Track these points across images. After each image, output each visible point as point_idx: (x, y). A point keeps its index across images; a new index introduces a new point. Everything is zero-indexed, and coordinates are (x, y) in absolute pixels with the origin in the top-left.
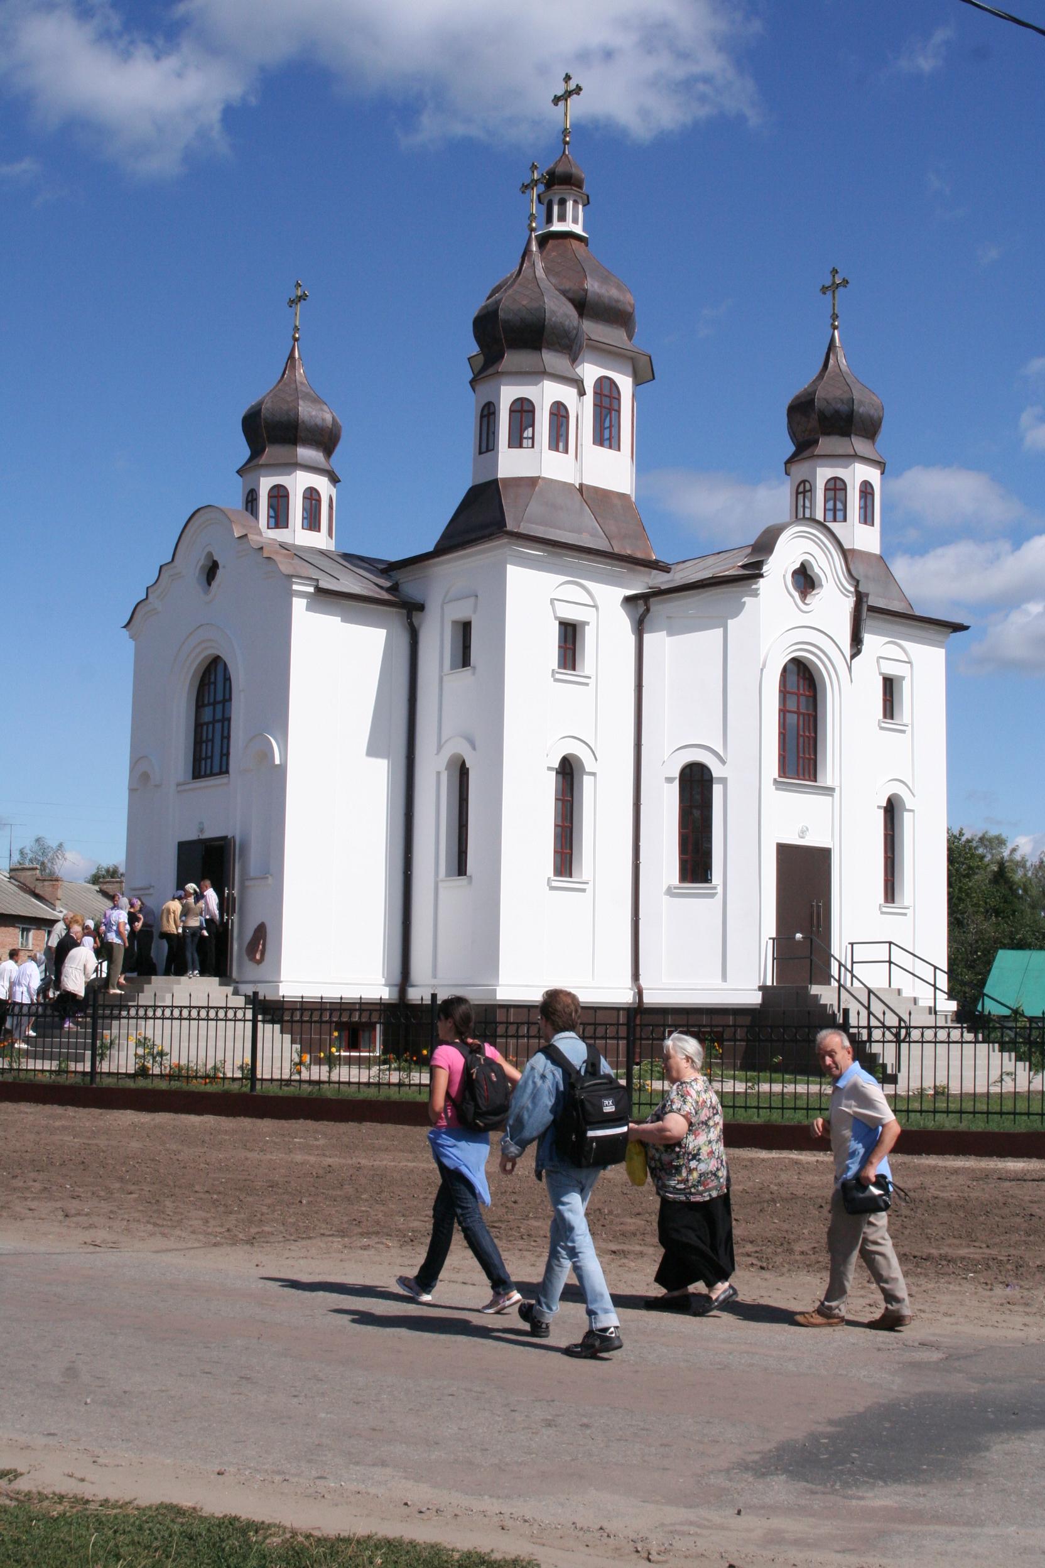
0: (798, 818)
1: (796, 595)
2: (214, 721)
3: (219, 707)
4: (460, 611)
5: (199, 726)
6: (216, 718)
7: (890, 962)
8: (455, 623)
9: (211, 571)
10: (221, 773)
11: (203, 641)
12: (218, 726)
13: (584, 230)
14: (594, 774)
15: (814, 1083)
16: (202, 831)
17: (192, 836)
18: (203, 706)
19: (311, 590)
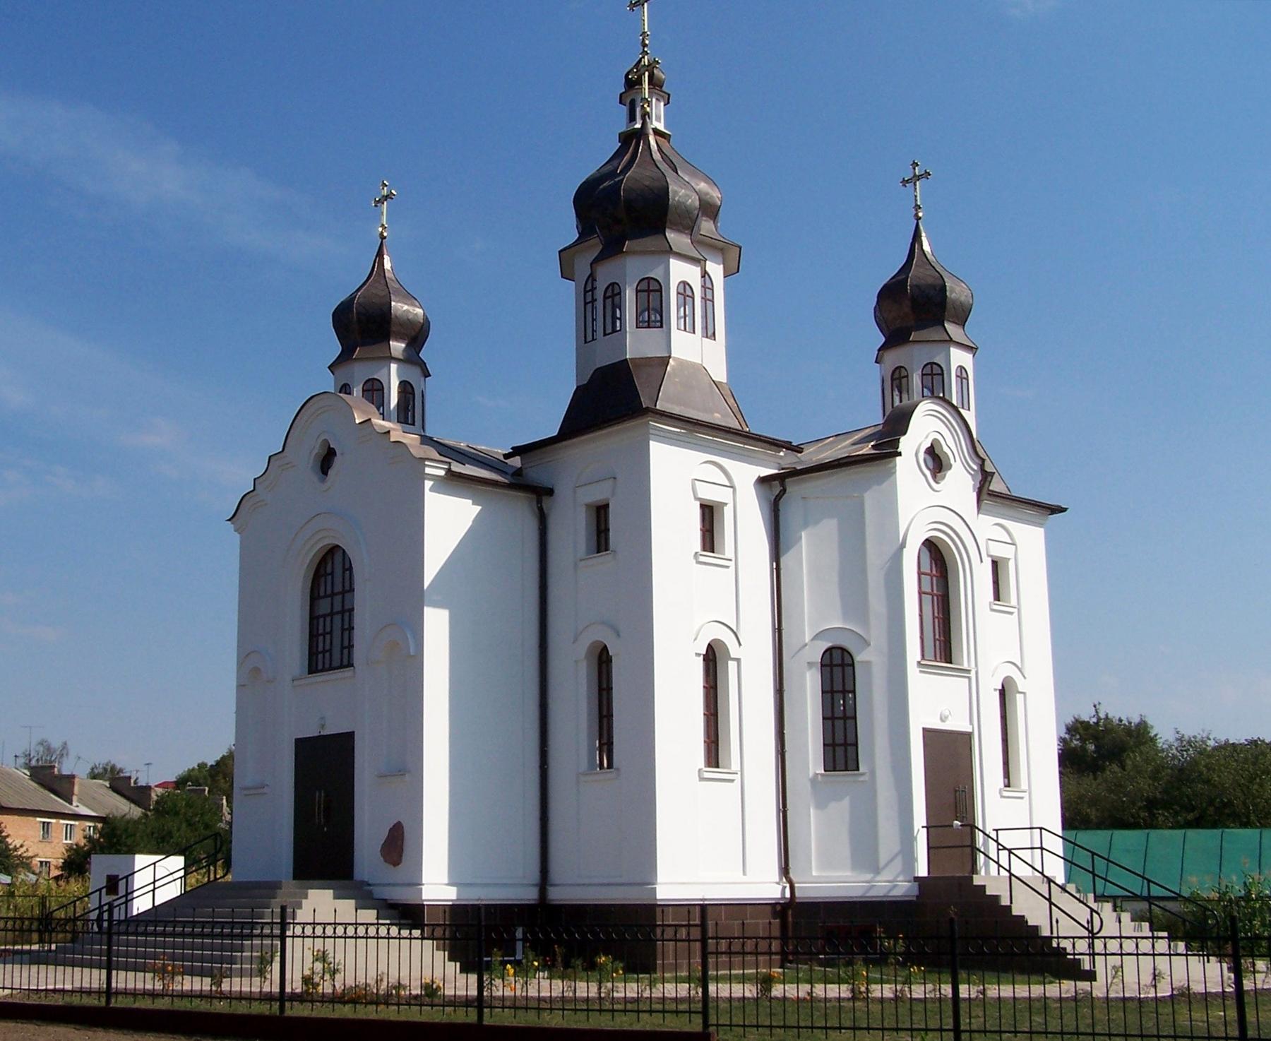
0: (934, 701)
1: (928, 473)
2: (332, 614)
3: (338, 599)
4: (596, 494)
5: (313, 618)
6: (332, 609)
7: (1042, 848)
8: (588, 506)
9: (327, 459)
10: (342, 666)
11: (916, 454)
12: (337, 618)
13: (665, 127)
14: (738, 660)
15: (1023, 983)
16: (323, 726)
17: (312, 732)
18: (319, 597)
19: (442, 473)
